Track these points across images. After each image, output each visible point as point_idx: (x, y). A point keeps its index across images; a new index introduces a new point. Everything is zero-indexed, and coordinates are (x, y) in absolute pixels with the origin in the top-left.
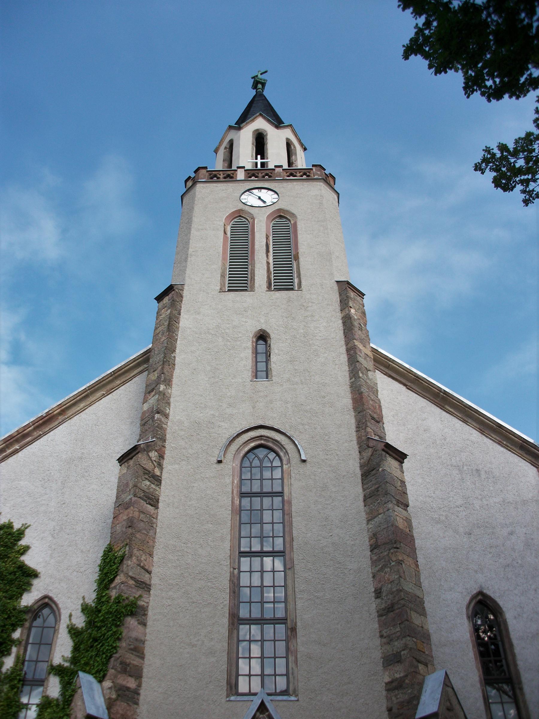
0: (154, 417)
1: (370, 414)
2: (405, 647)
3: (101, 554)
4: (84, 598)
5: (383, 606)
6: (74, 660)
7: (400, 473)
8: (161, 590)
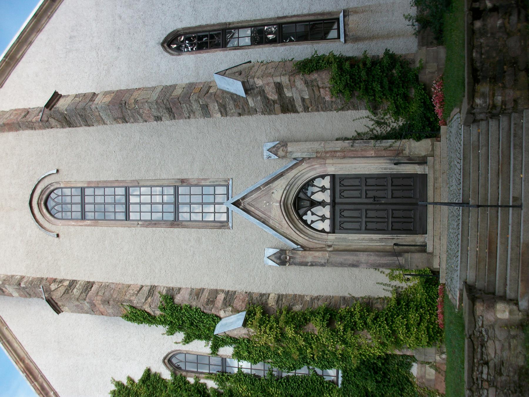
0: (23, 288)
1: (22, 118)
2: (197, 101)
3: (129, 322)
4: (163, 334)
5: (168, 116)
6: (207, 338)
7: (69, 97)
8: (154, 278)
